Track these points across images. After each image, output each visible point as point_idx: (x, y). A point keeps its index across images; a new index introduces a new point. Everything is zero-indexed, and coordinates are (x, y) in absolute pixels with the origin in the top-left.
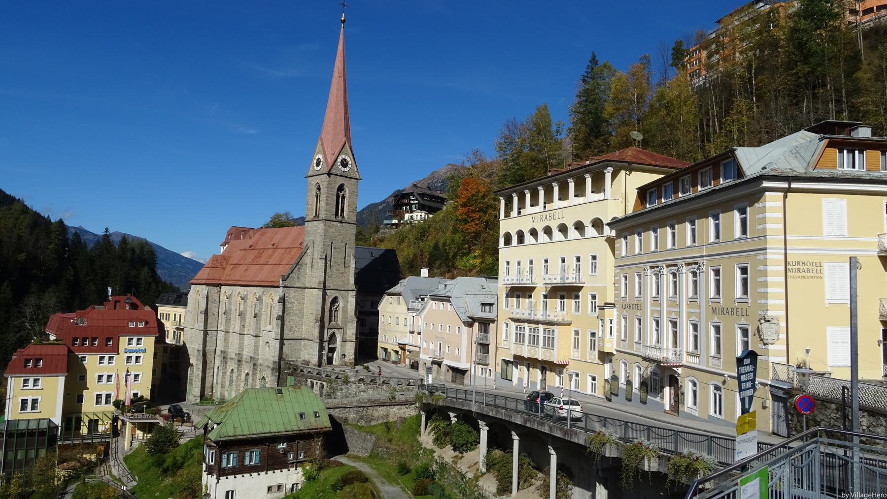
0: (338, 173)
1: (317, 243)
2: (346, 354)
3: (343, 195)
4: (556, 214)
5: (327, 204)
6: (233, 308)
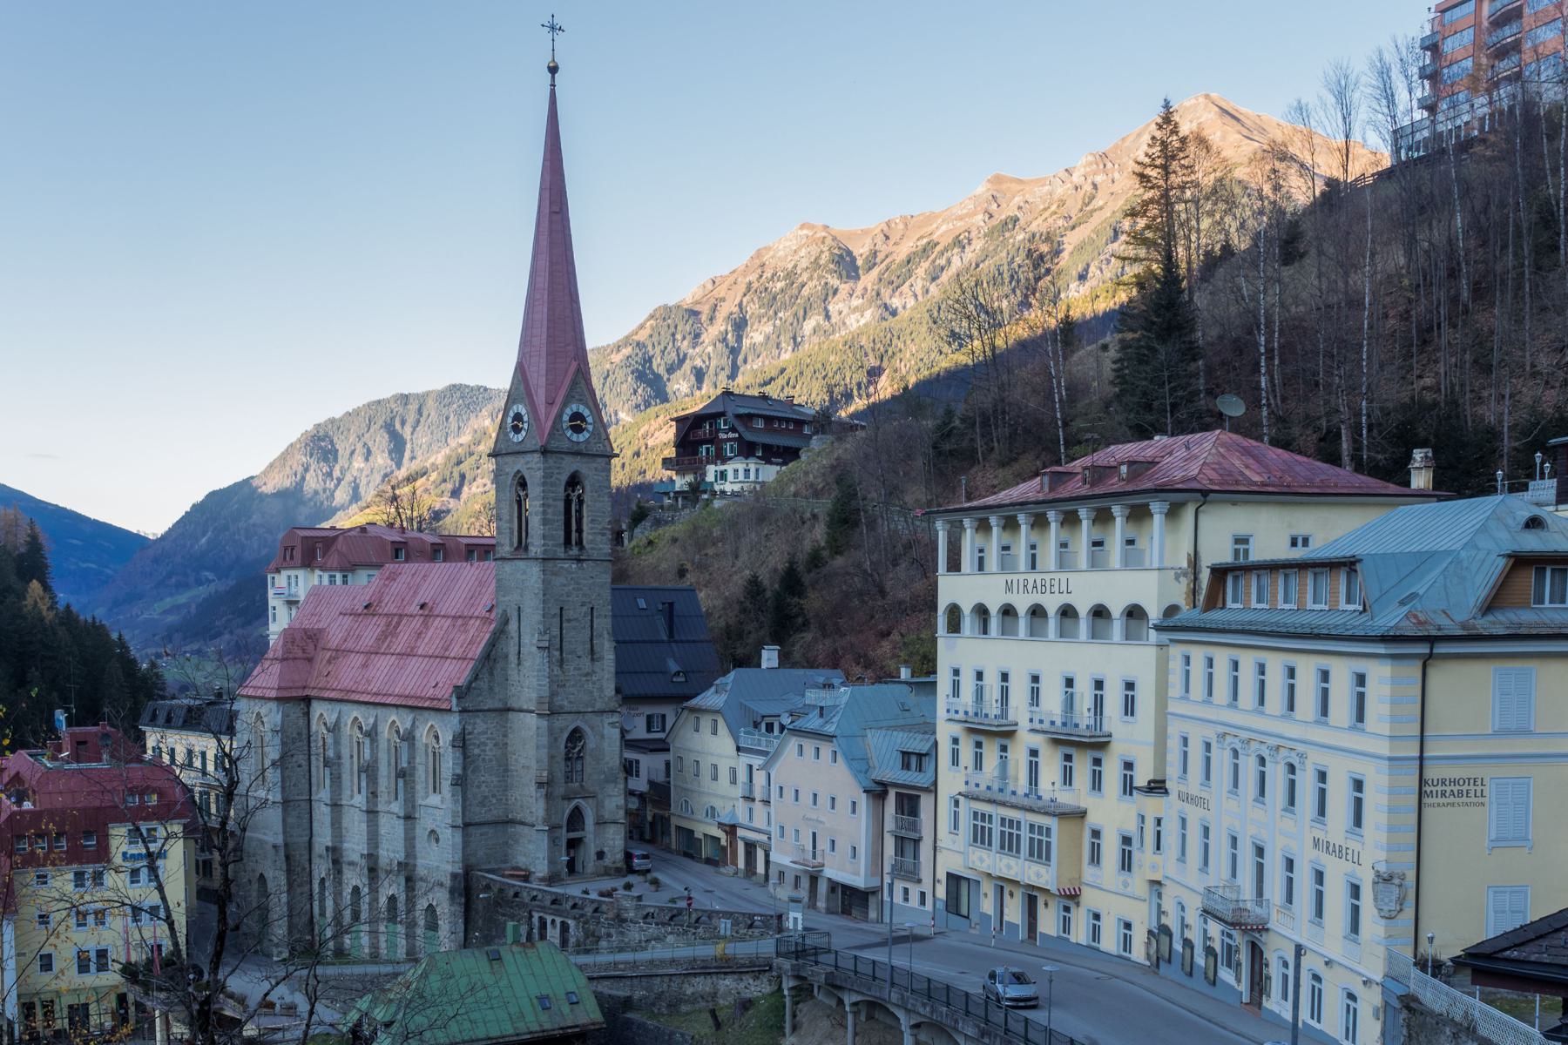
0: (565, 445)
1: (526, 611)
2: (606, 849)
3: (579, 496)
4: (1056, 583)
5: (545, 522)
6: (345, 752)
